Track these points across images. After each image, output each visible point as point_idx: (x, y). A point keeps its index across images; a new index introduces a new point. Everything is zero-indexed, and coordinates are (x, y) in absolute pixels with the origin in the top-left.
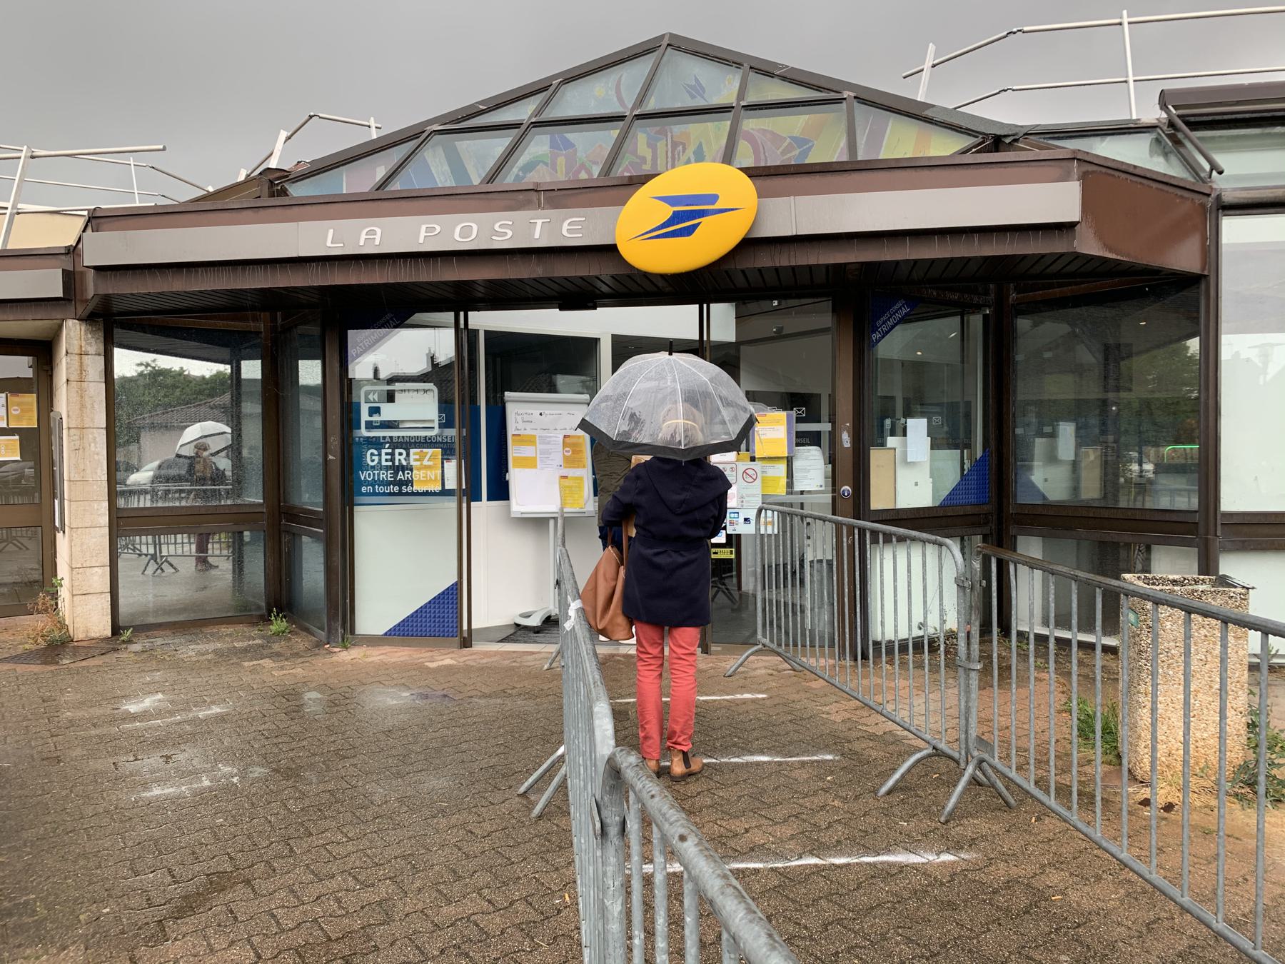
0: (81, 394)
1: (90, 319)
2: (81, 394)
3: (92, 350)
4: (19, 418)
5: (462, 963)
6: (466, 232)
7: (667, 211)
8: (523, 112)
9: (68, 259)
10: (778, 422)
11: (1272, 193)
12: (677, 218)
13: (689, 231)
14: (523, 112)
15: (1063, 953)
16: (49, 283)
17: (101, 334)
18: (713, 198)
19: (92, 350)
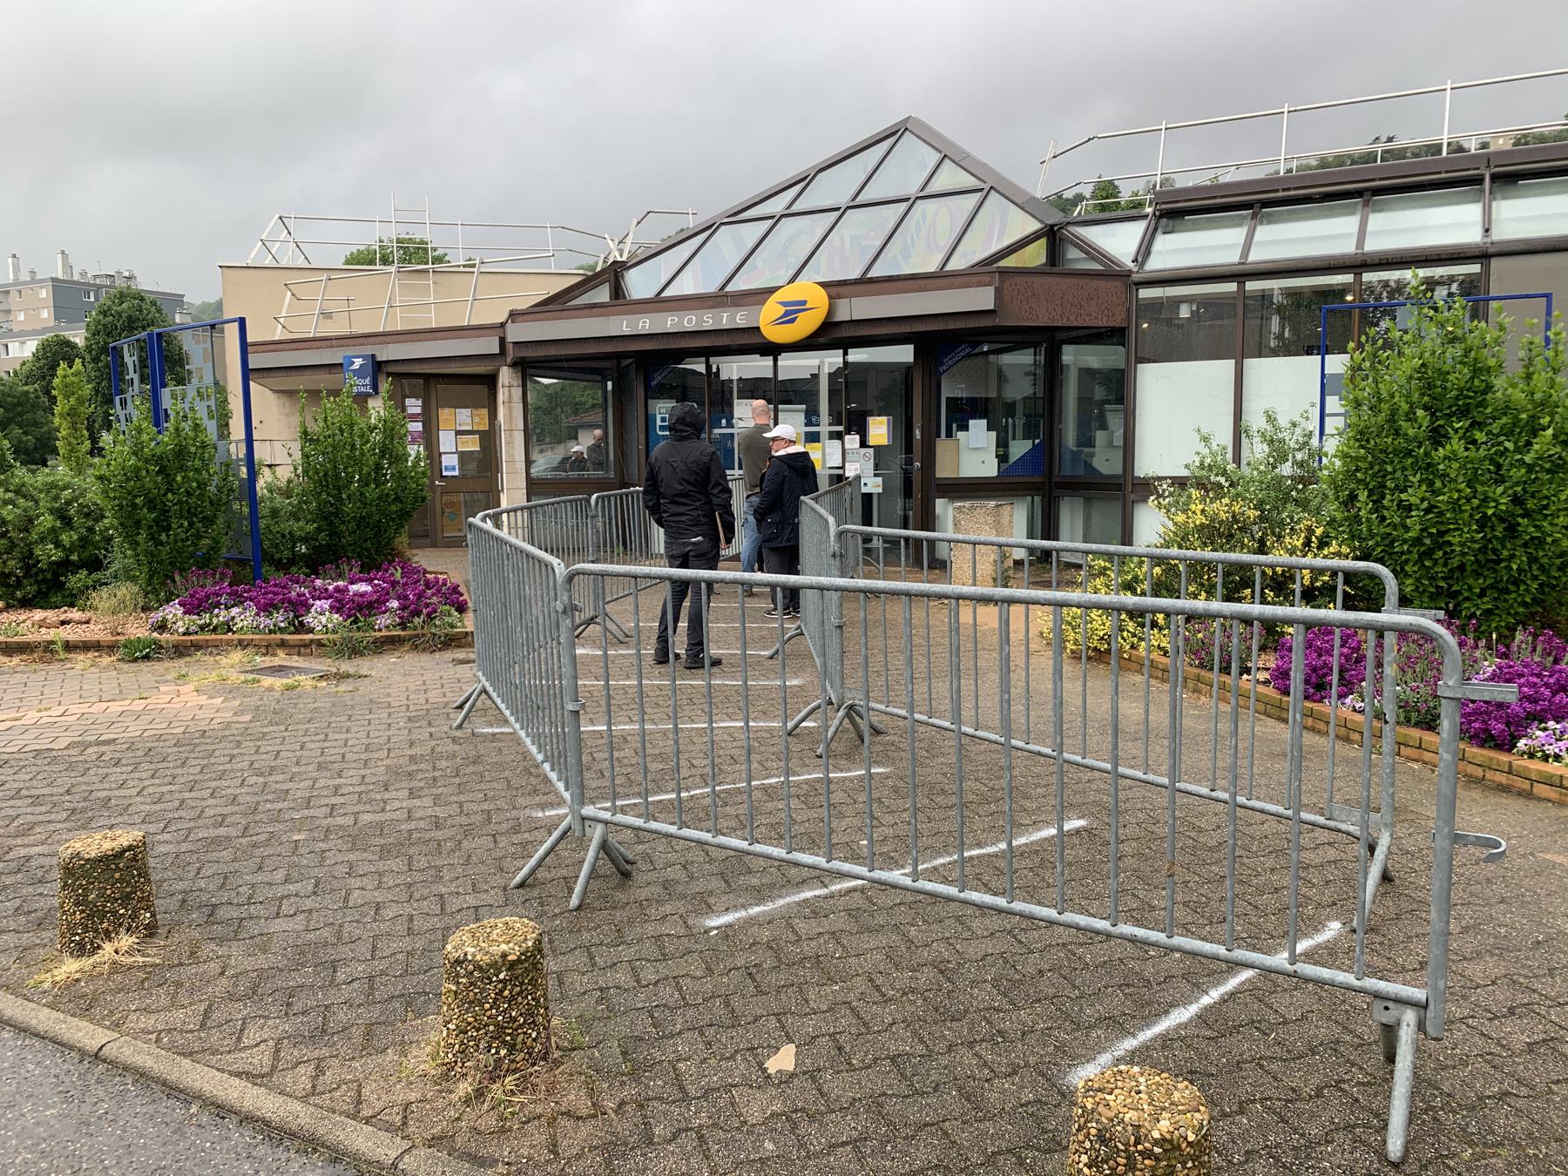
0: (510, 409)
1: (514, 365)
2: (510, 409)
3: (515, 384)
4: (478, 424)
5: (1565, 1099)
6: (690, 321)
7: (782, 310)
8: (776, 206)
9: (501, 330)
10: (882, 423)
11: (511, 462)
12: (787, 314)
13: (792, 321)
14: (776, 206)
15: (174, 480)
16: (490, 345)
17: (520, 374)
18: (804, 302)
19: (515, 384)
